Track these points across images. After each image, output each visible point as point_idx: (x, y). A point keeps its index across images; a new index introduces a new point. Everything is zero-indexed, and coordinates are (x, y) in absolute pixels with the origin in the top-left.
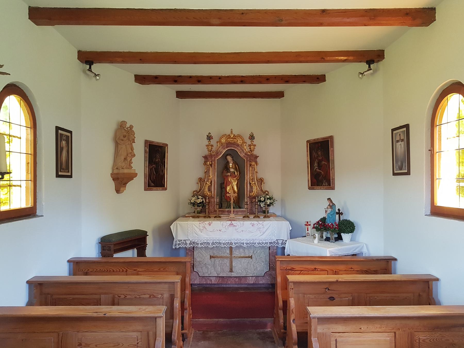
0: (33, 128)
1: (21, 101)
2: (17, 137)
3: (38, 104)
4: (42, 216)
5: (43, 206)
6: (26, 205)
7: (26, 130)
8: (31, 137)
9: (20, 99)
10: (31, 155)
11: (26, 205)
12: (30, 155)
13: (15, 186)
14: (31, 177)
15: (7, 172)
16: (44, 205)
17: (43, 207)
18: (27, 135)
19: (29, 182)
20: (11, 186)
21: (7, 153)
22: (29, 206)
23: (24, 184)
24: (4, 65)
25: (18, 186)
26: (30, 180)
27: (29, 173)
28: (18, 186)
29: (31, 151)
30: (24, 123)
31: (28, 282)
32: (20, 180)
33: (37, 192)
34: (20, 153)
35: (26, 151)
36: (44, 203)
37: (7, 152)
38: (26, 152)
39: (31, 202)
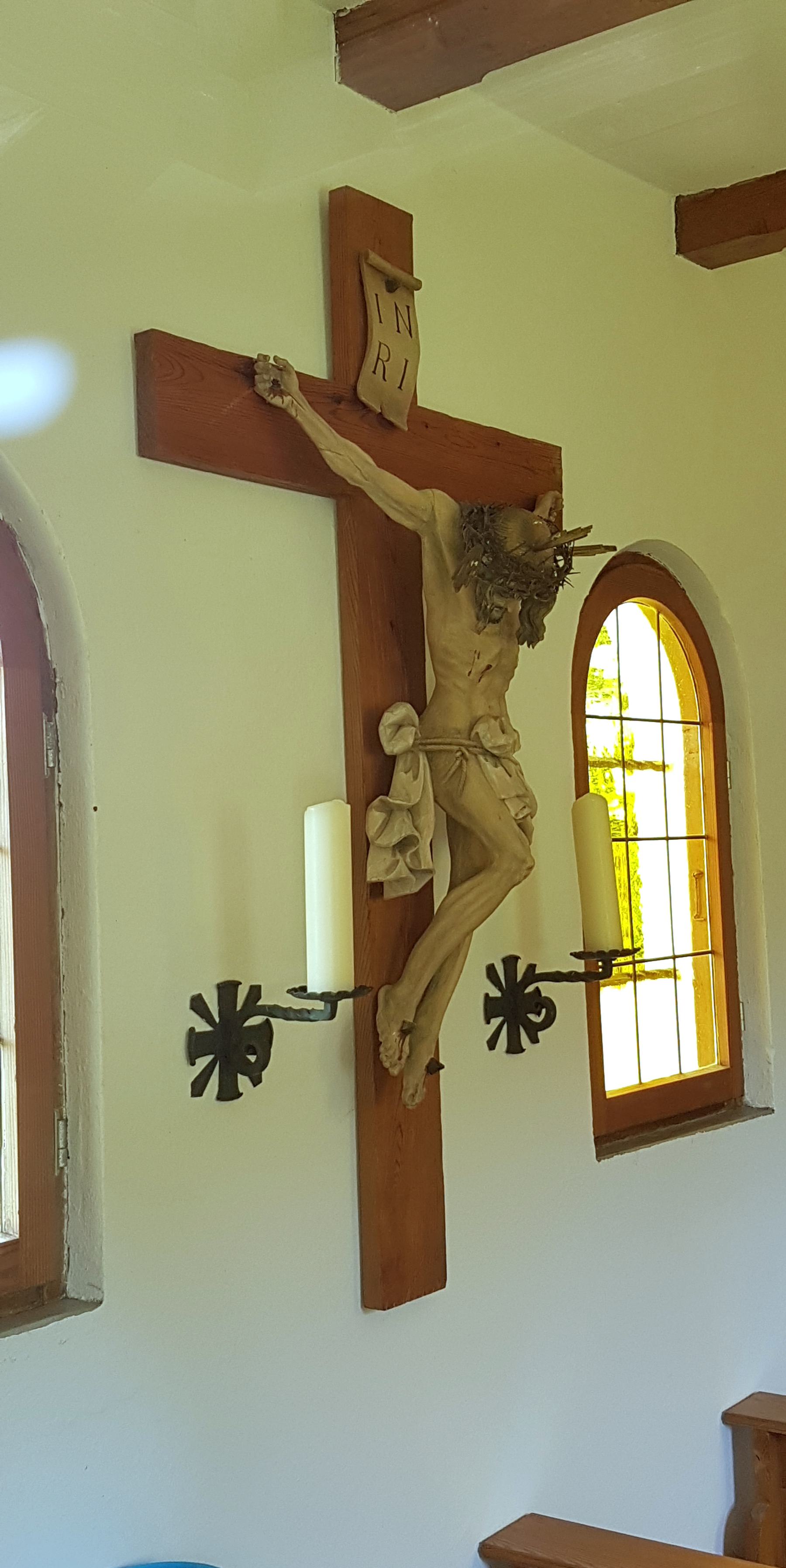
0: (711, 724)
1: (661, 616)
2: (651, 763)
3: (725, 613)
4: (767, 1108)
5: (769, 1063)
6: (693, 950)
7: (684, 731)
8: (705, 764)
9: (652, 605)
10: (711, 843)
11: (702, 1060)
12: (704, 840)
13: (652, 975)
14: (712, 936)
15: (624, 950)
16: (772, 1062)
17: (768, 1071)
18: (689, 752)
19: (703, 841)
20: (640, 976)
21: (619, 849)
22: (714, 1066)
23: (686, 967)
24: (591, 527)
25: (666, 974)
26: (710, 949)
27: (705, 920)
28: (666, 974)
29: (707, 825)
30: (674, 711)
31: (728, 1417)
32: (668, 839)
33: (741, 1000)
34: (668, 839)
35: (689, 826)
36: (772, 1054)
37: (614, 843)
38: (683, 717)
39: (720, 1049)
